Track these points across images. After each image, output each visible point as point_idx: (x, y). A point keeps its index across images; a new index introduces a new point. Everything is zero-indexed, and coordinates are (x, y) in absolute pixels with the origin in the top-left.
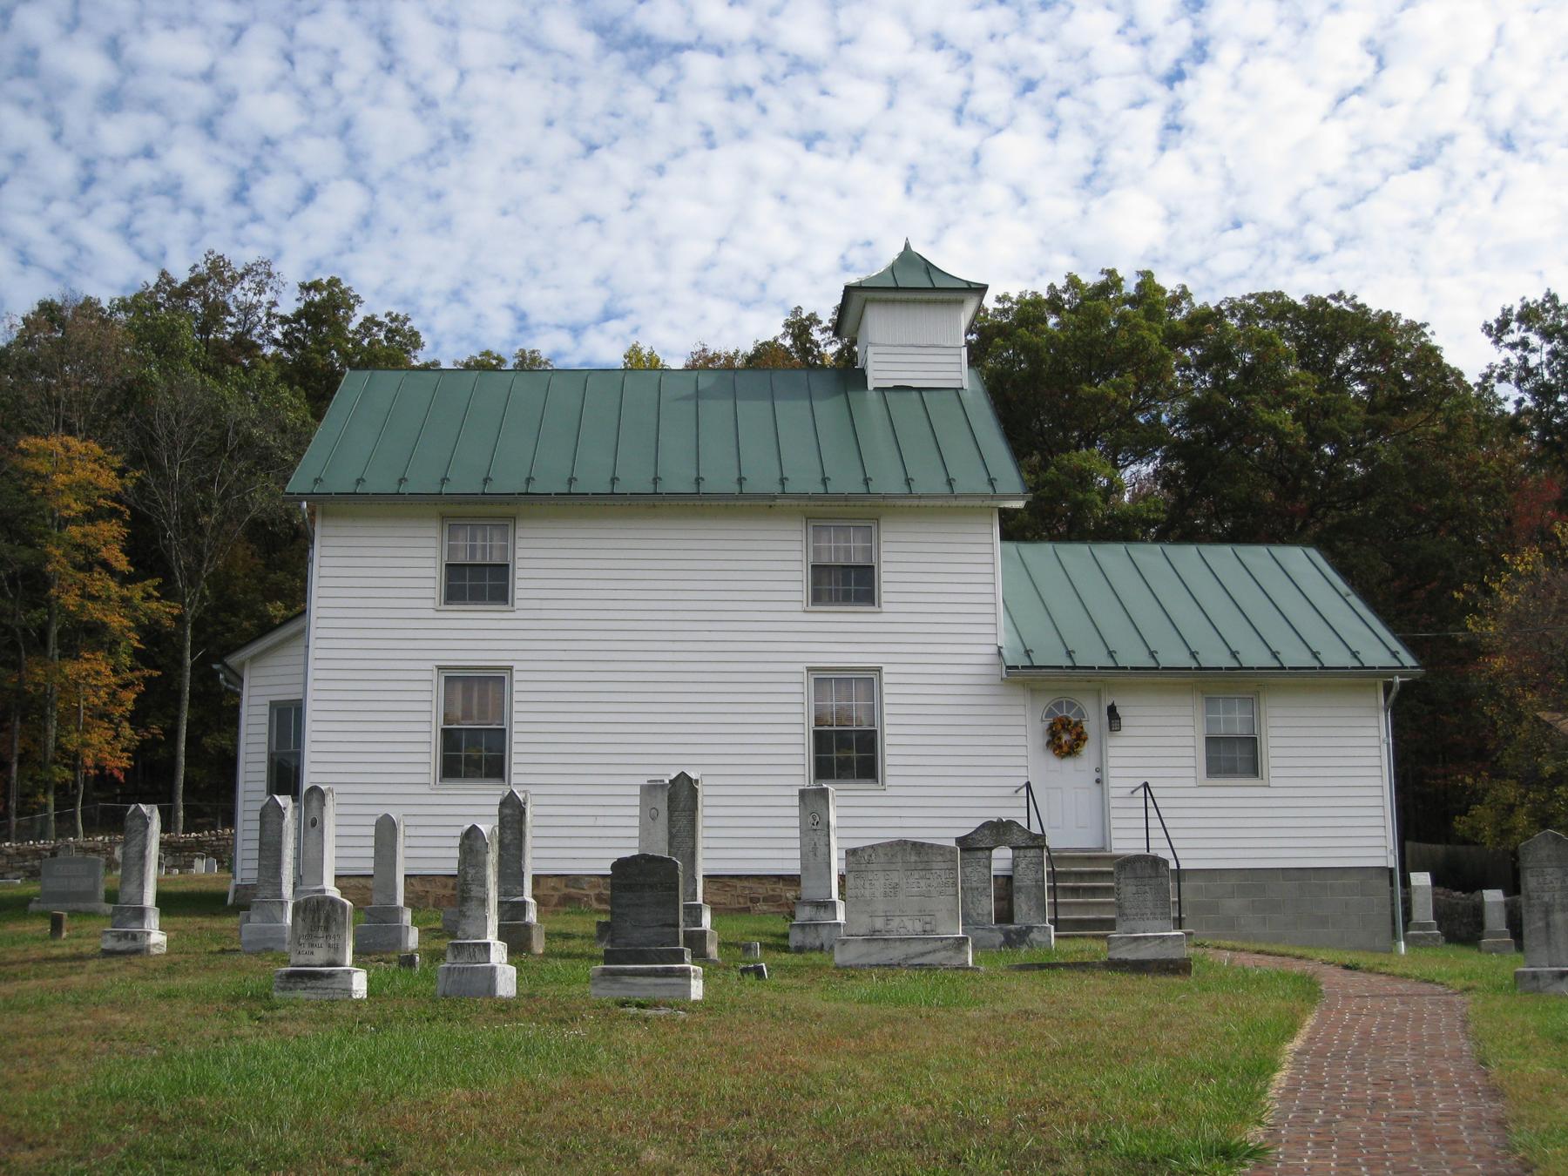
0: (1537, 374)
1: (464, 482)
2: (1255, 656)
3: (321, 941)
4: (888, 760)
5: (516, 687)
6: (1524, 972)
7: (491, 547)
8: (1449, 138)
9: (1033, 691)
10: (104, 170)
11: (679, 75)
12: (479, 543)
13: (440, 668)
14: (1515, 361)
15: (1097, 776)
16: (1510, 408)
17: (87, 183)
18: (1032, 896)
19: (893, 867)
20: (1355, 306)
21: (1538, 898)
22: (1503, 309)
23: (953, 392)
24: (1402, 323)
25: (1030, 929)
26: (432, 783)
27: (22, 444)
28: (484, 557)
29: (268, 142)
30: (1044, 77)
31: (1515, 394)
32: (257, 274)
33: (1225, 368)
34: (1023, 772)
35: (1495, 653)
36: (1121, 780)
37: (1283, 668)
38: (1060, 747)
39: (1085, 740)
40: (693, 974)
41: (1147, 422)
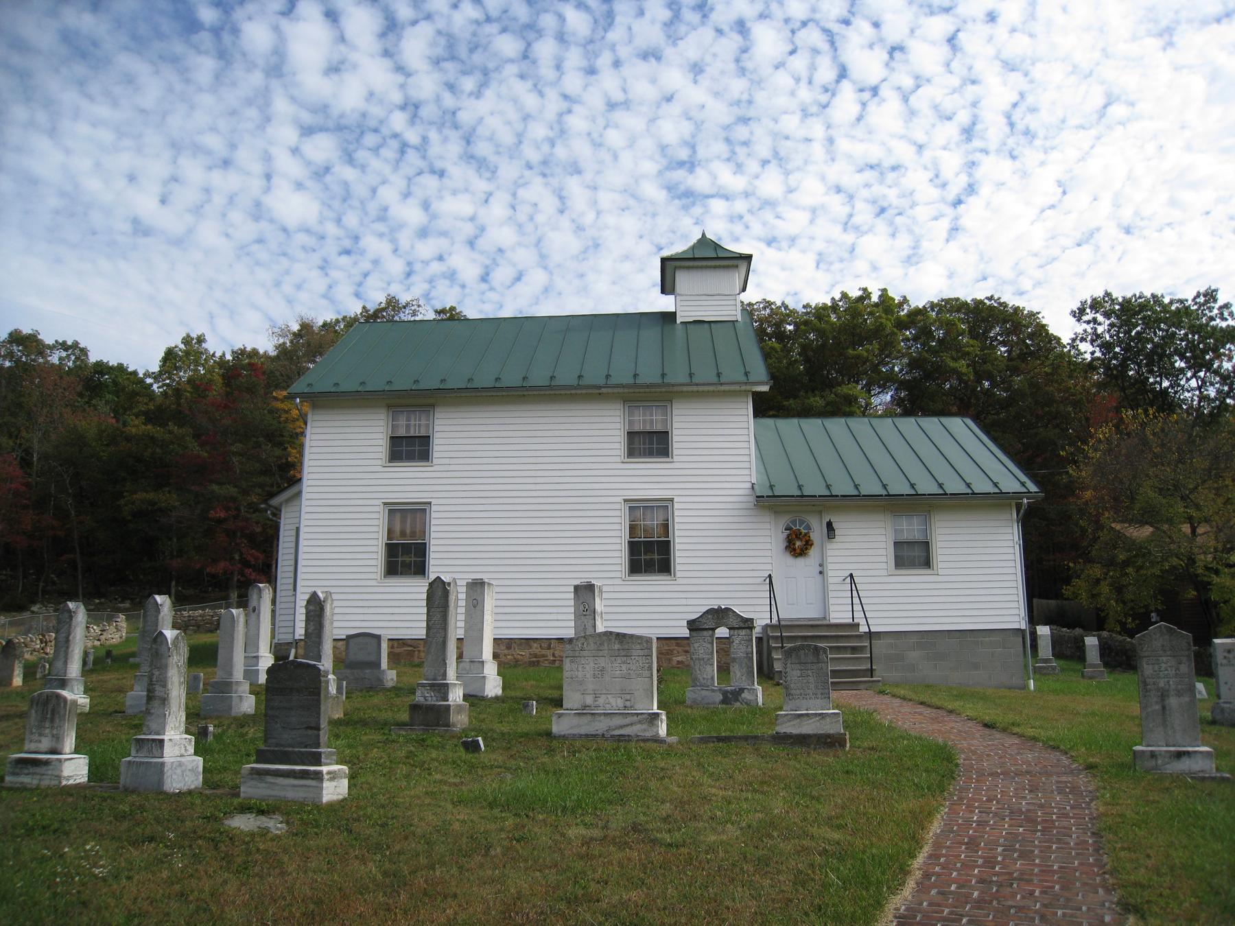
0: (1101, 338)
1: (402, 384)
2: (926, 486)
3: (47, 731)
4: (678, 560)
5: (433, 515)
6: (1143, 752)
7: (420, 425)
8: (1098, 229)
9: (775, 512)
10: (417, 267)
11: (707, 211)
12: (412, 422)
13: (385, 504)
14: (1089, 330)
15: (820, 569)
16: (1088, 357)
17: (409, 275)
18: (744, 665)
19: (601, 653)
20: (1001, 304)
21: (1154, 684)
22: (1081, 302)
23: (731, 324)
24: (1025, 312)
25: (742, 690)
26: (379, 579)
27: (274, 394)
28: (419, 432)
29: (501, 250)
30: (890, 206)
31: (1090, 349)
32: (413, 305)
33: (928, 339)
34: (769, 567)
35: (1084, 489)
36: (836, 573)
37: (946, 494)
38: (794, 550)
39: (812, 545)
40: (326, 777)
41: (887, 371)
